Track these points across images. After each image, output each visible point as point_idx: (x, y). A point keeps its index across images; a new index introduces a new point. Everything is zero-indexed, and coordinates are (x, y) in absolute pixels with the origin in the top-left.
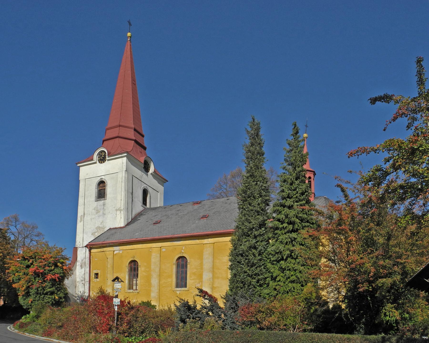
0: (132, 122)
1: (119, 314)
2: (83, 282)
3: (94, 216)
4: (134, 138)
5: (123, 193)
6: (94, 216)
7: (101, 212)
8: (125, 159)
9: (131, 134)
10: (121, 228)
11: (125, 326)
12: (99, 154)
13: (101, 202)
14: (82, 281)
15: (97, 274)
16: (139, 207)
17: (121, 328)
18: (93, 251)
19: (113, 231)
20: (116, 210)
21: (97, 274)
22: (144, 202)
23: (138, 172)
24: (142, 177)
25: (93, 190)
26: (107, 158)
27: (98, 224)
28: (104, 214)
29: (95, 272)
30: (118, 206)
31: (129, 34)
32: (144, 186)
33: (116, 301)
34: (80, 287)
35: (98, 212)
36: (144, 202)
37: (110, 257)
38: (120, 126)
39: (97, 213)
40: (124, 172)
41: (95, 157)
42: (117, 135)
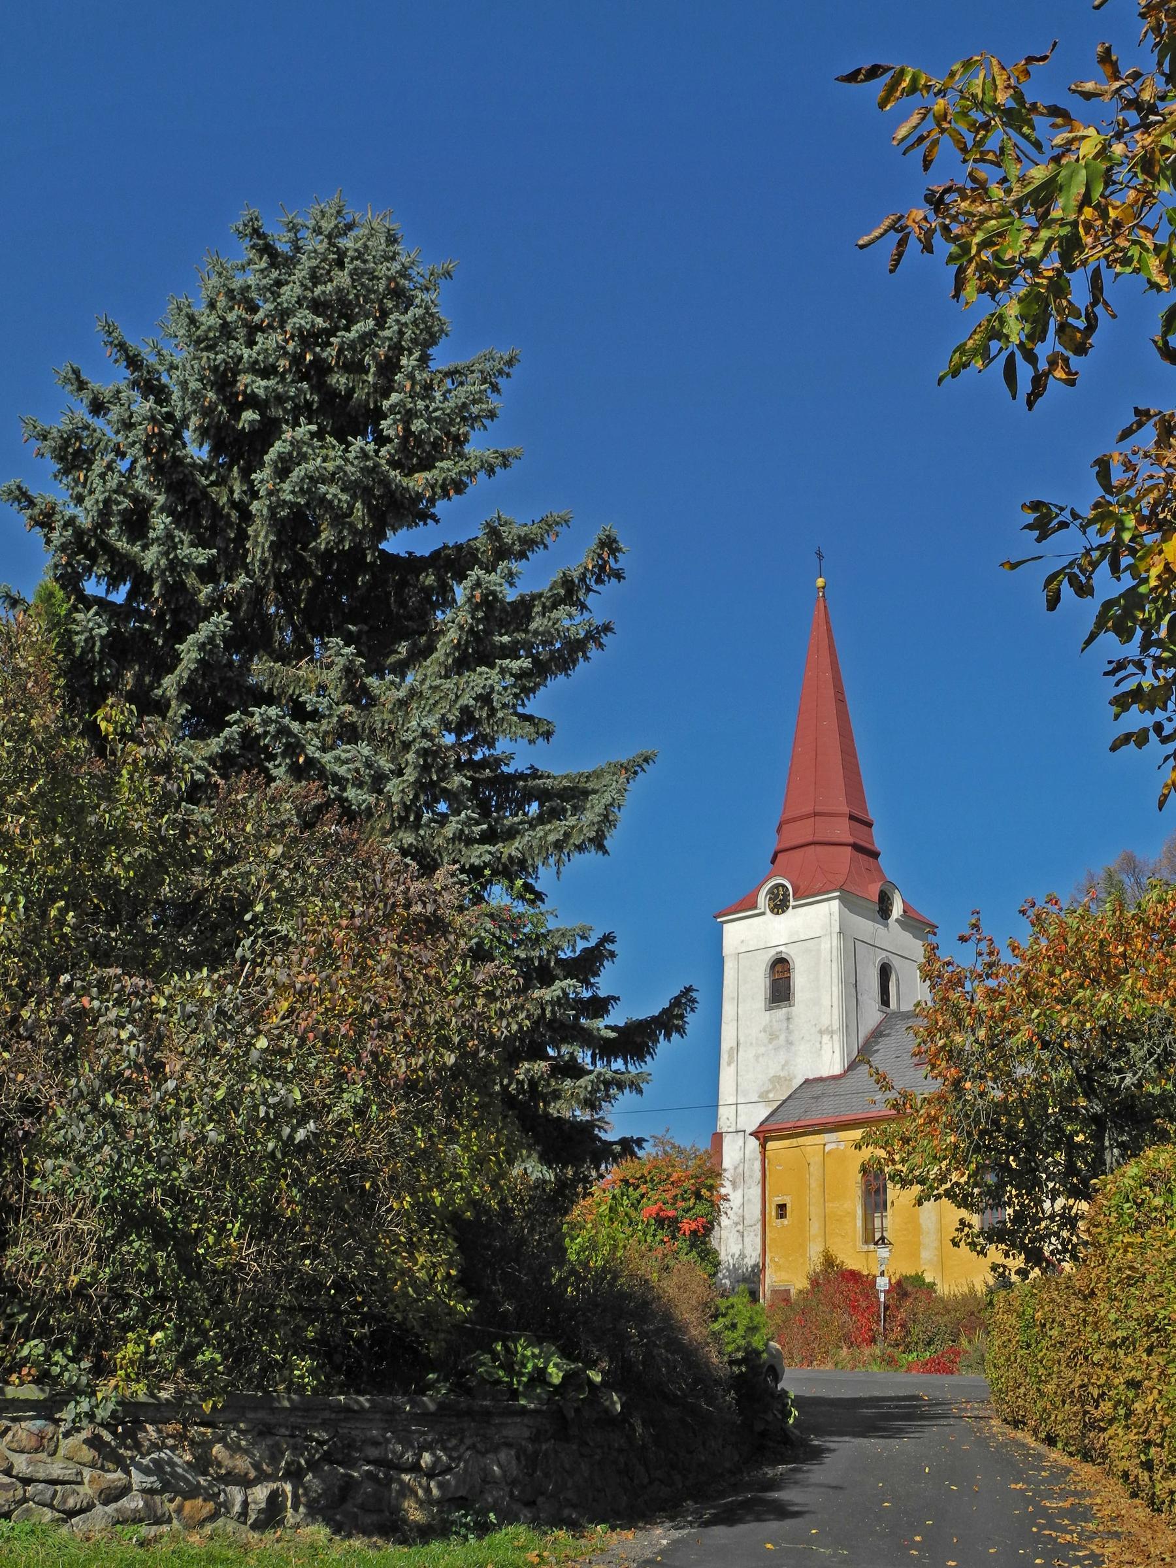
0: (843, 799)
1: (886, 1308)
2: (740, 1227)
3: (762, 1050)
4: (851, 840)
5: (835, 989)
6: (762, 1050)
7: (782, 1038)
8: (837, 902)
9: (842, 830)
10: (834, 1078)
11: (896, 1334)
12: (770, 891)
13: (781, 1013)
14: (737, 1224)
15: (782, 1207)
16: (872, 1015)
17: (893, 1337)
18: (770, 1145)
19: (817, 1089)
20: (821, 1032)
21: (782, 1207)
22: (885, 1001)
23: (866, 927)
24: (874, 935)
25: (758, 982)
26: (792, 903)
27: (774, 1069)
28: (790, 1043)
29: (779, 1200)
30: (825, 1021)
31: (820, 582)
32: (881, 957)
33: (882, 1283)
34: (732, 1241)
35: (773, 1037)
36: (885, 1001)
37: (816, 1159)
38: (815, 814)
39: (771, 1041)
40: (835, 936)
41: (762, 899)
42: (810, 839)
